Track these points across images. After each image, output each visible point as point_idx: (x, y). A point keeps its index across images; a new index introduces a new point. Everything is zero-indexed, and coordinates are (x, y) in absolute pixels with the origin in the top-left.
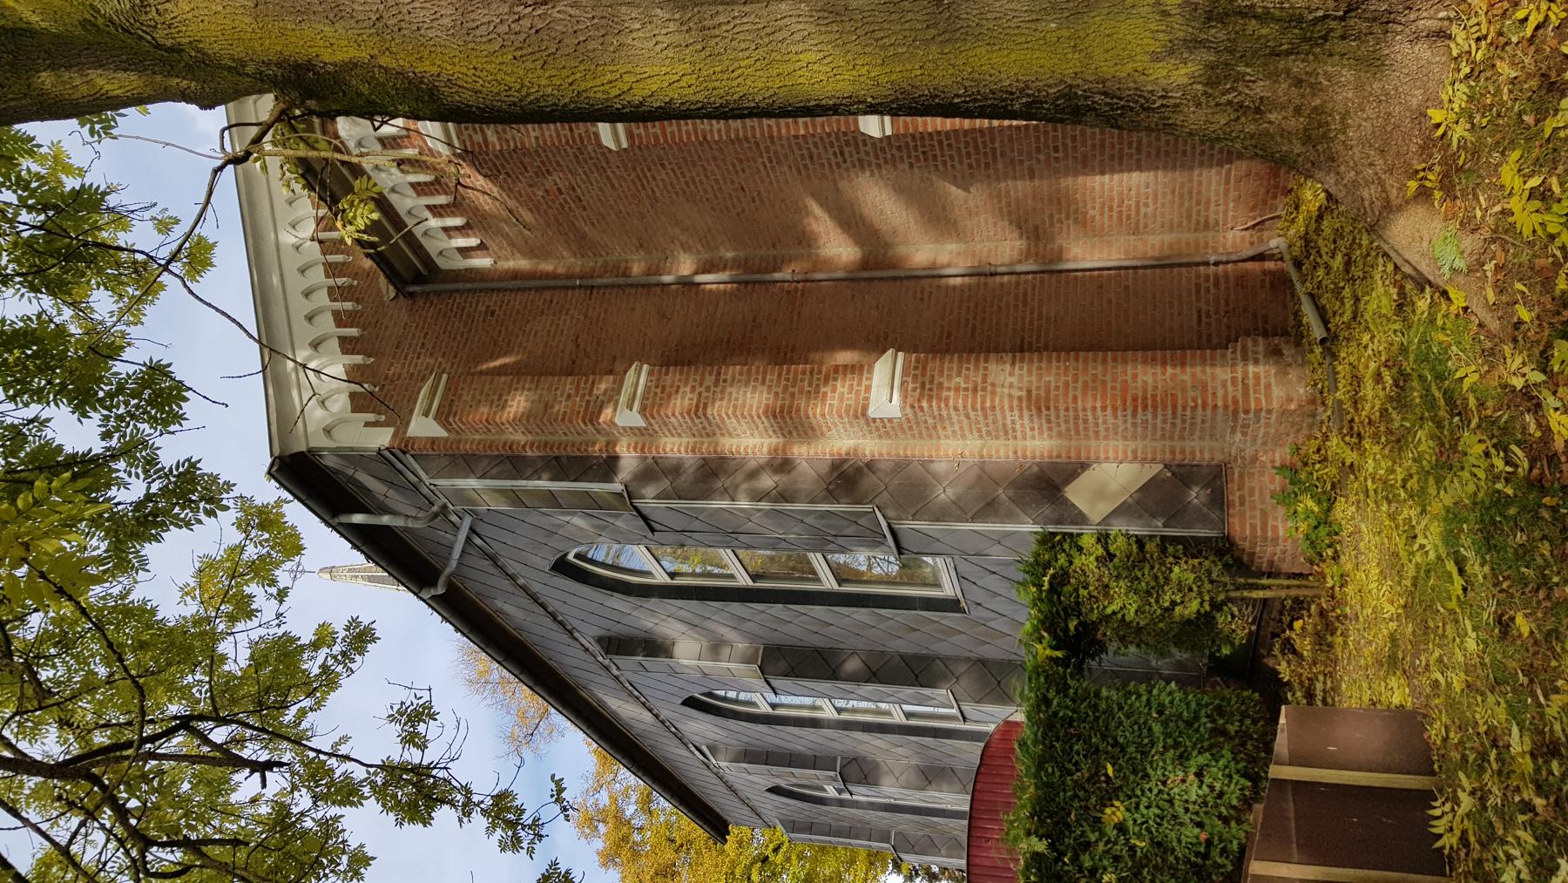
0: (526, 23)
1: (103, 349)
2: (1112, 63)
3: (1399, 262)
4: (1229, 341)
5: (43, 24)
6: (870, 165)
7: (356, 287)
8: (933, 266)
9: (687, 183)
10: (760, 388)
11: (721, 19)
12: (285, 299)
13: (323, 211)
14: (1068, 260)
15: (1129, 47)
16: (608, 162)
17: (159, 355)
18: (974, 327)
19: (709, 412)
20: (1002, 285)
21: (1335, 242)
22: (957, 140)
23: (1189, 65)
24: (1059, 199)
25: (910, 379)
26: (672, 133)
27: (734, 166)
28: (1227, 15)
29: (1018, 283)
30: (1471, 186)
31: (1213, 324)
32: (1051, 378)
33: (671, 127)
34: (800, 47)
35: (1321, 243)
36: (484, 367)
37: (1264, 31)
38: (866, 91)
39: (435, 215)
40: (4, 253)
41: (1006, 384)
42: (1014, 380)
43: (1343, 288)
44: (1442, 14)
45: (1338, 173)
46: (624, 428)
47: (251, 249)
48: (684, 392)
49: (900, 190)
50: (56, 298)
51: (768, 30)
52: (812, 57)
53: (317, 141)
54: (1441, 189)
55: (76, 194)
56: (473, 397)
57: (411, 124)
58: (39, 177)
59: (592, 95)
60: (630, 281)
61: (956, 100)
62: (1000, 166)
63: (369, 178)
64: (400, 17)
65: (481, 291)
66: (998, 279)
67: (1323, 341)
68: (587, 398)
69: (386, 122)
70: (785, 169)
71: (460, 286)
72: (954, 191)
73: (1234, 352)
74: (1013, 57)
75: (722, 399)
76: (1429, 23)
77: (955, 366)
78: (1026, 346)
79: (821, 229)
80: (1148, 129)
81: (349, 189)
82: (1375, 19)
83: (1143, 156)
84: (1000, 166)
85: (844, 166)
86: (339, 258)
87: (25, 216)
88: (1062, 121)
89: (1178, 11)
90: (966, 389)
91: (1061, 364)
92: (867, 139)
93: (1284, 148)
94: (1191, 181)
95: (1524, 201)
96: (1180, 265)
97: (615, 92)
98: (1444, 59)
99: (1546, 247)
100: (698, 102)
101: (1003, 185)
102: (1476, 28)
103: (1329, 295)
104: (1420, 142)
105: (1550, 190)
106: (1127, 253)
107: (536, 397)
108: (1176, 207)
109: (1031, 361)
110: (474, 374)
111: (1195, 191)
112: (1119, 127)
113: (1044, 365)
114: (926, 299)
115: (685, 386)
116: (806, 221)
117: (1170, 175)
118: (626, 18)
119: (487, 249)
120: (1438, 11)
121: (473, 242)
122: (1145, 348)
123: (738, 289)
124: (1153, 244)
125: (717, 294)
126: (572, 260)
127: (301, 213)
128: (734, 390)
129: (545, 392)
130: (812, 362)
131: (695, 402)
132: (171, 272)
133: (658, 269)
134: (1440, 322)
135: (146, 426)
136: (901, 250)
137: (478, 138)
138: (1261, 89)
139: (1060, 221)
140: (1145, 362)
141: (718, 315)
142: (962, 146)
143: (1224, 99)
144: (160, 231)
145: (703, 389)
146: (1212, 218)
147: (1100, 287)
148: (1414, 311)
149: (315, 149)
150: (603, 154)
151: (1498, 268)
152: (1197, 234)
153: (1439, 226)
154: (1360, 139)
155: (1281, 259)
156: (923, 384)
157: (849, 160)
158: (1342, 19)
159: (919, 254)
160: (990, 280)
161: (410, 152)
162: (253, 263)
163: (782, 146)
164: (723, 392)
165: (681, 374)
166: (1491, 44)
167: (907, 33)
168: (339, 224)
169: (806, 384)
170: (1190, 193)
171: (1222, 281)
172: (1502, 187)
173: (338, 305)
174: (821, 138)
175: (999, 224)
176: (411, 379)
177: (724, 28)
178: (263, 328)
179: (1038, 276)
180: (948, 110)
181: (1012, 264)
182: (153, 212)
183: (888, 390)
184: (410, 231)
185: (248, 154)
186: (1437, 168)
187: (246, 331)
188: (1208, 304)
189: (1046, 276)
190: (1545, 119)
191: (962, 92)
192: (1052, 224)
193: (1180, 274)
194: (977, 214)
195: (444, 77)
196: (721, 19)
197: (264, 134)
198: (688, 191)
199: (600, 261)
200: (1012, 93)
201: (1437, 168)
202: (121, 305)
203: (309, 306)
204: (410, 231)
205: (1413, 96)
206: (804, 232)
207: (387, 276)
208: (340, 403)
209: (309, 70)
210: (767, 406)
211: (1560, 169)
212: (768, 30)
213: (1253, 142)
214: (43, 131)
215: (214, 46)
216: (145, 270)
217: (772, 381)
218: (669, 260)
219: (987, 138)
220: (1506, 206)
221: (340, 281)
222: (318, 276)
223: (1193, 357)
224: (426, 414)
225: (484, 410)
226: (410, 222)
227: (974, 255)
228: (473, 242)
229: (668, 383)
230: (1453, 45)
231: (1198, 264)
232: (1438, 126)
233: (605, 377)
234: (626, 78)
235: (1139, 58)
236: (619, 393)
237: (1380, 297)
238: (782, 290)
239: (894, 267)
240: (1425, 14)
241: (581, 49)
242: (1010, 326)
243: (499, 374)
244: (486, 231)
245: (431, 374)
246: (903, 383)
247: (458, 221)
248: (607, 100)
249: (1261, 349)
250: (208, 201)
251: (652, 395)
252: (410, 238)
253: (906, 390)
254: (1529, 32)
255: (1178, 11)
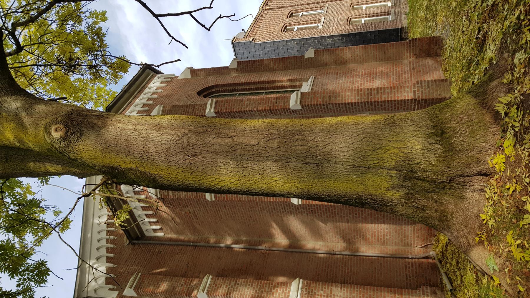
0: (187, 161)
1: (26, 254)
2: (374, 190)
3: (475, 265)
4: (417, 287)
5: (35, 149)
6: (294, 213)
7: (116, 240)
8: (314, 249)
9: (232, 213)
10: (250, 288)
11: (249, 165)
12: (91, 242)
13: (111, 213)
14: (360, 252)
15: (379, 185)
16: (207, 205)
17: (44, 258)
18: (327, 272)
19: (231, 295)
20: (337, 258)
21: (452, 255)
22: (323, 208)
23: (399, 193)
24: (357, 231)
25: (304, 290)
26: (230, 197)
27: (249, 209)
28: (411, 178)
29: (343, 259)
30: (497, 241)
31: (412, 280)
32: (355, 295)
33: (229, 196)
34: (273, 176)
35: (447, 255)
36: (154, 271)
37: (424, 184)
38: (294, 190)
39: (147, 217)
40: (2, 219)
41: (339, 295)
42: (342, 294)
43: (457, 272)
44: (481, 184)
45: (451, 232)
46: (293, 111)
47: (84, 224)
48: (223, 287)
49: (303, 222)
50: (15, 234)
51: (263, 170)
52: (277, 179)
53: (114, 191)
54: (487, 241)
55: (31, 201)
56: (148, 283)
57: (145, 188)
58: (20, 194)
59: (205, 184)
60: (209, 245)
61: (323, 196)
62: (337, 218)
63: (128, 204)
64: (148, 156)
65: (158, 244)
66: (336, 256)
67: (451, 290)
68: (188, 286)
69: (137, 187)
70: (265, 211)
71: (151, 242)
72: (322, 225)
73: (420, 291)
74: (342, 185)
75: (236, 291)
76: (477, 187)
77: (320, 286)
78: (346, 282)
79: (276, 233)
80: (386, 212)
81: (121, 208)
82: (460, 184)
83: (385, 219)
84: (337, 218)
85: (285, 212)
86: (112, 229)
87: (12, 207)
88: (358, 206)
89: (395, 176)
90: (324, 296)
91: (358, 290)
92: (293, 205)
93: (432, 222)
94: (402, 229)
95: (516, 248)
96: (399, 258)
97: (213, 184)
98: (484, 198)
99: (526, 265)
100: (239, 189)
101: (338, 224)
102: (493, 190)
103: (451, 274)
104: (478, 225)
105: (524, 245)
106: (380, 251)
107: (170, 284)
108: (397, 237)
109: (347, 288)
110: (150, 274)
111: (403, 232)
112: (377, 210)
113: (352, 289)
114: (311, 260)
115: (224, 285)
116: (271, 229)
117: (394, 226)
118: (219, 162)
119: (163, 230)
120: (480, 183)
121: (158, 227)
122: (388, 287)
123: (246, 251)
124: (390, 249)
125: (239, 252)
126: (191, 236)
127: (102, 213)
128: (241, 288)
129: (174, 283)
130: (270, 280)
131: (227, 291)
132: (56, 231)
133: (219, 241)
134: (491, 288)
135: (33, 283)
136: (303, 243)
137: (166, 194)
138: (423, 202)
139: (357, 238)
140: (388, 292)
141: (238, 260)
142: (325, 210)
143: (411, 205)
144: (55, 215)
145: (230, 287)
146: (409, 242)
147: (372, 263)
148: (482, 283)
149: (112, 194)
150: (206, 202)
151: (510, 271)
152: (404, 248)
153: (488, 254)
154: (458, 222)
155: (434, 259)
156: (309, 292)
157: (287, 211)
158: (449, 183)
159: (309, 244)
160: (333, 256)
161: (143, 197)
162: (83, 228)
163: (265, 204)
164: (237, 288)
165: (223, 280)
166: (499, 195)
167: (308, 174)
168: (115, 219)
169: (267, 288)
170: (402, 233)
171: (414, 265)
172: (508, 243)
173: (108, 245)
174: (278, 203)
175: (337, 237)
176: (128, 273)
177: (250, 168)
178: (81, 252)
179: (350, 256)
180: (320, 199)
181: (341, 251)
182: (54, 209)
183: (296, 293)
184: (138, 223)
185: (90, 194)
186: (485, 234)
187: (76, 253)
188: (409, 272)
189: (353, 257)
190: (519, 221)
191: (325, 194)
192: (355, 239)
193: (399, 261)
194: (329, 233)
195: (159, 175)
196: (249, 165)
197: (97, 188)
198: (232, 216)
199: (200, 237)
200: (341, 196)
201: (485, 234)
202: (35, 239)
203: (98, 245)
204: (138, 223)
205: (475, 209)
206: (270, 233)
207: (127, 237)
208: (102, 281)
209: (116, 170)
210: (252, 295)
211: (527, 239)
212: (263, 170)
213: (422, 219)
214: (25, 180)
215: (86, 160)
216: (47, 228)
217: (255, 286)
218: (224, 239)
219: (333, 208)
220: (510, 249)
221: (112, 237)
222: (104, 235)
223: (405, 292)
224: (131, 287)
225: (151, 288)
226: (139, 219)
227: (328, 247)
228: (158, 227)
229: (218, 282)
230: (486, 194)
231: (405, 258)
232: (484, 220)
233: (196, 279)
234: (217, 180)
235: (383, 189)
236: (200, 286)
237: (470, 277)
238: (261, 252)
239: (301, 248)
240: (476, 184)
241: (204, 170)
242: (340, 273)
243: (159, 275)
244: (163, 224)
245: (135, 272)
246: (302, 291)
247: (154, 220)
248: (210, 186)
249: (429, 291)
250: (74, 208)
251: (211, 287)
252: (138, 226)
253: (303, 294)
254: (511, 192)
255: (395, 176)
